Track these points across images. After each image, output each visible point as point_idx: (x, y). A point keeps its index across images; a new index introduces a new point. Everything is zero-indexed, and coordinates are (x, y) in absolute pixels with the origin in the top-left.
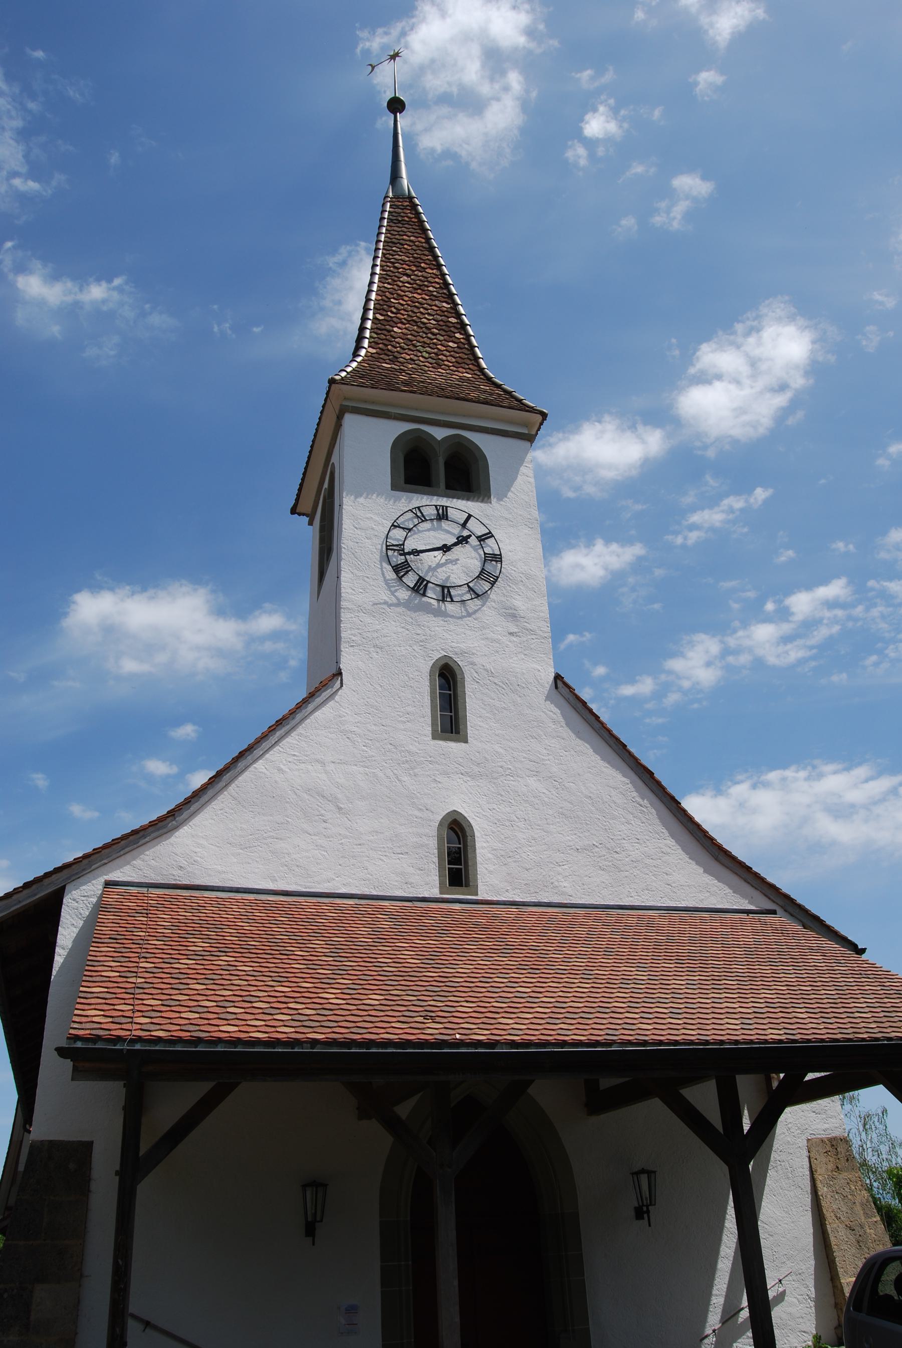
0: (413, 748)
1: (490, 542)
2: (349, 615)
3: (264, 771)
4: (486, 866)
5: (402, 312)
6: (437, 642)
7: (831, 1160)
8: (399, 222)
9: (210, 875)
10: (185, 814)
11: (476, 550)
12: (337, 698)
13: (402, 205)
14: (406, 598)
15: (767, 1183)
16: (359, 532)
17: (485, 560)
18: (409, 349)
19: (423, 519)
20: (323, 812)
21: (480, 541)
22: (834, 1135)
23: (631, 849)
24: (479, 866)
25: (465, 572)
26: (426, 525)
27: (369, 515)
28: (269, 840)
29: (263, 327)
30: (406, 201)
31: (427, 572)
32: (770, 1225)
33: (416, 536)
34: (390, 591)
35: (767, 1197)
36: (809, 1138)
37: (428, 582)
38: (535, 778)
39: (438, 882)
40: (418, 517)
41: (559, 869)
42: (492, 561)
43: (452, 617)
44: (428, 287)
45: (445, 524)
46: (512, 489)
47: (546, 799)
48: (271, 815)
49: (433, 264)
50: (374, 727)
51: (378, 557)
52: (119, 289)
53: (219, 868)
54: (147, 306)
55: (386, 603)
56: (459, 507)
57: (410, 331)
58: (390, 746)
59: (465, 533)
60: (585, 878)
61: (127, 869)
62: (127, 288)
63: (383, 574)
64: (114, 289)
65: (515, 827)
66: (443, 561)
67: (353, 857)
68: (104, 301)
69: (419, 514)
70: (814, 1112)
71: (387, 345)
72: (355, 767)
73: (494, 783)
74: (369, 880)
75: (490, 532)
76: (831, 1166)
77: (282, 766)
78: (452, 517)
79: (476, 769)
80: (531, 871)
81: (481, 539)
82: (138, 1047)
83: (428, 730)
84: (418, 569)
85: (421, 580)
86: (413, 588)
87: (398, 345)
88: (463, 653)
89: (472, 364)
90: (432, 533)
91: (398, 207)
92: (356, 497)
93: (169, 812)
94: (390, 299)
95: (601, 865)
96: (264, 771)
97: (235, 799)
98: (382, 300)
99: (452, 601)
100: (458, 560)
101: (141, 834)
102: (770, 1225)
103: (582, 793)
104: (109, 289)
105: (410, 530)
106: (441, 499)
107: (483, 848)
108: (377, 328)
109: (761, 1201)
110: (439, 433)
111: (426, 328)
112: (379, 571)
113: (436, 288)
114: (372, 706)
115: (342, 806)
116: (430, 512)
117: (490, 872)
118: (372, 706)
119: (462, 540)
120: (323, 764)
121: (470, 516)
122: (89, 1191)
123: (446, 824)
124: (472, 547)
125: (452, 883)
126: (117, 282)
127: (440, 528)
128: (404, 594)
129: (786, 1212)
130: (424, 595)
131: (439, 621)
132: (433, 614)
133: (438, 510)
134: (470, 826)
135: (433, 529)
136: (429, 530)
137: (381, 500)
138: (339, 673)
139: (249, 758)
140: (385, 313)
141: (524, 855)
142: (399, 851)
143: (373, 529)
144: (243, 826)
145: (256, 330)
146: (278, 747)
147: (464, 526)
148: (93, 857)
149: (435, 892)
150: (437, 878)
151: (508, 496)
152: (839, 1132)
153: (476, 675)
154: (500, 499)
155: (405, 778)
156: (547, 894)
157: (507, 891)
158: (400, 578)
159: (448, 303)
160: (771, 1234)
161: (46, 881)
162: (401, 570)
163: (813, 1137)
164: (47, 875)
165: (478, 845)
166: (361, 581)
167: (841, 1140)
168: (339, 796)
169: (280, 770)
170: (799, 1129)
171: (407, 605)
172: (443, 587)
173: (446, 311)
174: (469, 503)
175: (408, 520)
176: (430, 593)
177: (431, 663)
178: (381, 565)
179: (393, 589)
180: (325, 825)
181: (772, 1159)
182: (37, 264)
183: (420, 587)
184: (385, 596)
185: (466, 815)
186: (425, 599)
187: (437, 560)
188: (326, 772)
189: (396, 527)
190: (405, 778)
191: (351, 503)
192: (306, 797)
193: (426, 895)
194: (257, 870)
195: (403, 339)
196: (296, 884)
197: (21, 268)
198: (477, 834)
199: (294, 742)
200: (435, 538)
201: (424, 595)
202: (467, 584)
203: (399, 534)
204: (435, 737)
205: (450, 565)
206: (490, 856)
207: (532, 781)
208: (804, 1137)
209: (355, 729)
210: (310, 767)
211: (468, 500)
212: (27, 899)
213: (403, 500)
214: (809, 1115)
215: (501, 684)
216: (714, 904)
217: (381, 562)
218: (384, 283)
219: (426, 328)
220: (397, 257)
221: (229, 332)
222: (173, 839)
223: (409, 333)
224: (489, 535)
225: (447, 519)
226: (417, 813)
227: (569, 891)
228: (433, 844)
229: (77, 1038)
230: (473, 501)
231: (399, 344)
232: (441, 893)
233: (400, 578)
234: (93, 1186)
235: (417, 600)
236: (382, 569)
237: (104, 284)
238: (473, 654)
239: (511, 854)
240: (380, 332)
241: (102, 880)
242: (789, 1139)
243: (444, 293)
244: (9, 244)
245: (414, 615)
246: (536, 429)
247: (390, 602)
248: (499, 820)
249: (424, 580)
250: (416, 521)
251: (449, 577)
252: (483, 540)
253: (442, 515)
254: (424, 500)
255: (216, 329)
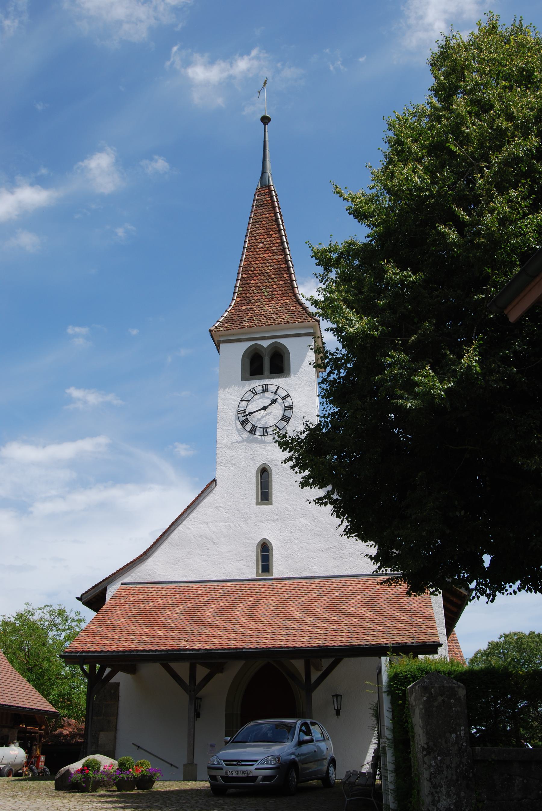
0: (247, 511)
1: (288, 399)
2: (220, 450)
3: (182, 530)
4: (278, 562)
5: (257, 269)
6: (260, 457)
8: (261, 206)
9: (161, 577)
10: (150, 553)
11: (281, 405)
12: (214, 492)
13: (264, 193)
14: (247, 437)
16: (225, 407)
17: (285, 410)
18: (258, 293)
19: (255, 394)
20: (207, 545)
21: (283, 400)
23: (350, 547)
24: (274, 562)
25: (275, 418)
26: (257, 396)
27: (230, 397)
28: (185, 560)
29: (365, 57)
30: (266, 189)
31: (257, 422)
33: (252, 403)
34: (239, 435)
37: (257, 427)
38: (304, 518)
39: (255, 572)
40: (253, 393)
41: (313, 560)
42: (288, 409)
43: (268, 443)
44: (272, 247)
45: (266, 394)
46: (302, 366)
47: (309, 528)
49: (276, 230)
50: (230, 503)
51: (234, 418)
52: (257, 58)
53: (164, 574)
54: (279, 65)
55: (237, 442)
56: (273, 383)
57: (259, 280)
58: (237, 511)
59: (276, 397)
61: (129, 578)
62: (261, 55)
63: (236, 426)
64: (253, 58)
65: (293, 543)
66: (265, 414)
67: (219, 564)
68: (248, 70)
69: (254, 391)
71: (246, 294)
72: (221, 523)
73: (284, 523)
74: (225, 573)
75: (288, 394)
77: (190, 527)
78: (270, 389)
79: (276, 517)
80: (299, 563)
81: (284, 398)
82: (84, 654)
83: (254, 501)
84: (252, 421)
85: (254, 426)
86: (249, 432)
87: (252, 292)
88: (272, 461)
89: (291, 292)
90: (260, 400)
91: (261, 195)
92: (224, 389)
93: (144, 552)
94: (251, 262)
95: (333, 557)
96: (182, 530)
97: (170, 543)
98: (247, 264)
99: (268, 435)
100: (272, 412)
101: (134, 562)
103: (327, 522)
104: (250, 60)
105: (249, 401)
106: (265, 380)
107: (276, 554)
108: (243, 284)
110: (265, 344)
111: (269, 276)
112: (234, 425)
113: (276, 247)
114: (229, 493)
115: (215, 541)
116: (259, 389)
117: (280, 565)
118: (229, 493)
119: (274, 401)
120: (207, 523)
121: (278, 387)
122: (118, 700)
123: (260, 545)
124: (279, 404)
125: (263, 571)
126: (254, 53)
127: (264, 397)
128: (246, 435)
130: (254, 434)
131: (262, 446)
132: (258, 443)
133: (263, 387)
134: (271, 544)
135: (261, 398)
136: (258, 399)
137: (236, 388)
138: (214, 480)
139: (176, 525)
140: (247, 272)
141: (296, 556)
142: (239, 559)
143: (232, 404)
144: (174, 555)
145: (361, 60)
146: (188, 519)
147: (275, 393)
148: (116, 574)
149: (254, 576)
150: (255, 570)
151: (300, 371)
153: (278, 471)
154: (295, 374)
155: (243, 526)
156: (306, 573)
157: (287, 573)
158: (244, 427)
159: (282, 255)
161: (100, 585)
162: (244, 423)
164: (100, 583)
165: (274, 553)
166: (226, 432)
168: (214, 537)
169: (189, 529)
171: (247, 441)
172: (263, 428)
173: (281, 261)
174: (279, 379)
175: (249, 396)
176: (257, 433)
177: (256, 468)
178: (236, 422)
179: (240, 433)
180: (207, 551)
182: (197, 57)
183: (253, 431)
184: (237, 438)
185: (269, 540)
186: (255, 436)
187: (261, 414)
188: (208, 527)
189: (243, 401)
190: (243, 526)
191: (222, 392)
192: (199, 539)
193: (250, 578)
194: (179, 573)
195: (255, 287)
196: (195, 577)
197: (188, 63)
198: (274, 548)
199: (195, 515)
200: (262, 403)
201: (254, 434)
202: (275, 425)
203: (244, 404)
204: (257, 504)
205: (267, 416)
206: (280, 557)
207: (302, 520)
209: (221, 505)
210: (201, 526)
211: (279, 378)
212: (94, 593)
213: (247, 385)
215: (290, 473)
217: (235, 420)
218: (249, 252)
219: (269, 276)
220: (258, 231)
221: (342, 67)
222: (146, 563)
223: (259, 281)
224: (288, 396)
225: (267, 391)
226: (248, 541)
227: (317, 571)
228: (254, 554)
229: (66, 652)
230: (281, 378)
231: (253, 291)
232: (256, 576)
233: (244, 427)
234: (120, 699)
235: (252, 437)
236: (236, 424)
237: (246, 58)
238: (277, 460)
239: (290, 556)
240: (244, 286)
241: (120, 583)
243: (280, 249)
244: (175, 49)
245: (250, 445)
246: (319, 329)
247: (239, 440)
248: (285, 540)
249: (255, 426)
250: (252, 395)
251: (267, 422)
252: (285, 399)
253: (265, 390)
254: (257, 383)
255: (332, 68)
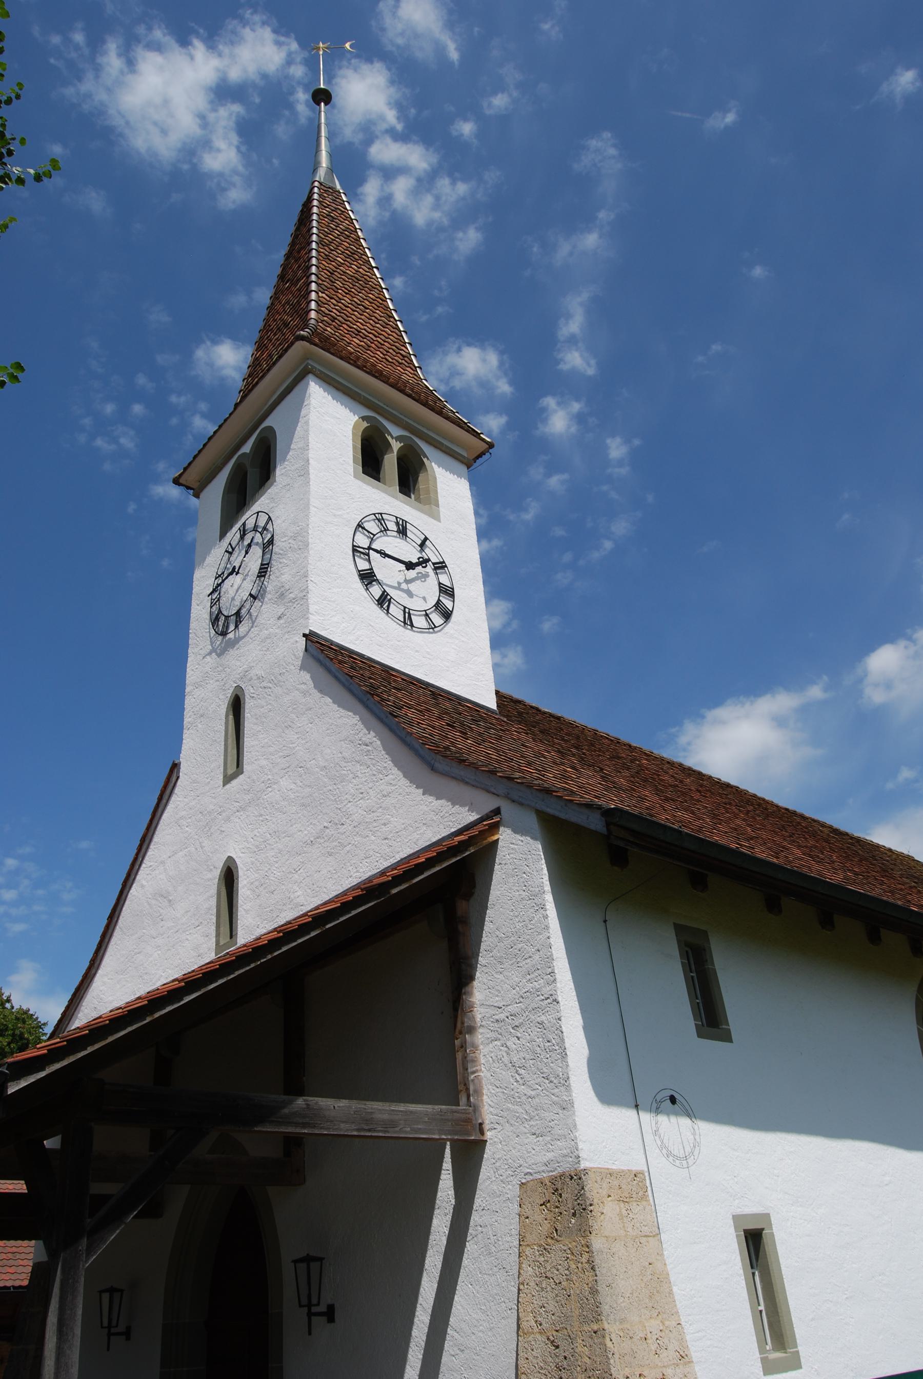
7: (549, 1217)
15: (463, 1264)
22: (560, 1170)
32: (462, 1334)
35: (433, 1290)
36: (524, 1181)
48: (137, 933)
60: (316, 875)
70: (535, 1134)
76: (547, 1226)
102: (462, 1334)
109: (454, 1294)
129: (484, 1312)
152: (568, 1162)
160: (462, 1348)
163: (529, 1178)
167: (572, 1178)
170: (510, 1167)
181: (472, 1223)
202: (425, 611)
208: (516, 1182)
214: (526, 1141)
216: (429, 840)
242: (495, 1188)
